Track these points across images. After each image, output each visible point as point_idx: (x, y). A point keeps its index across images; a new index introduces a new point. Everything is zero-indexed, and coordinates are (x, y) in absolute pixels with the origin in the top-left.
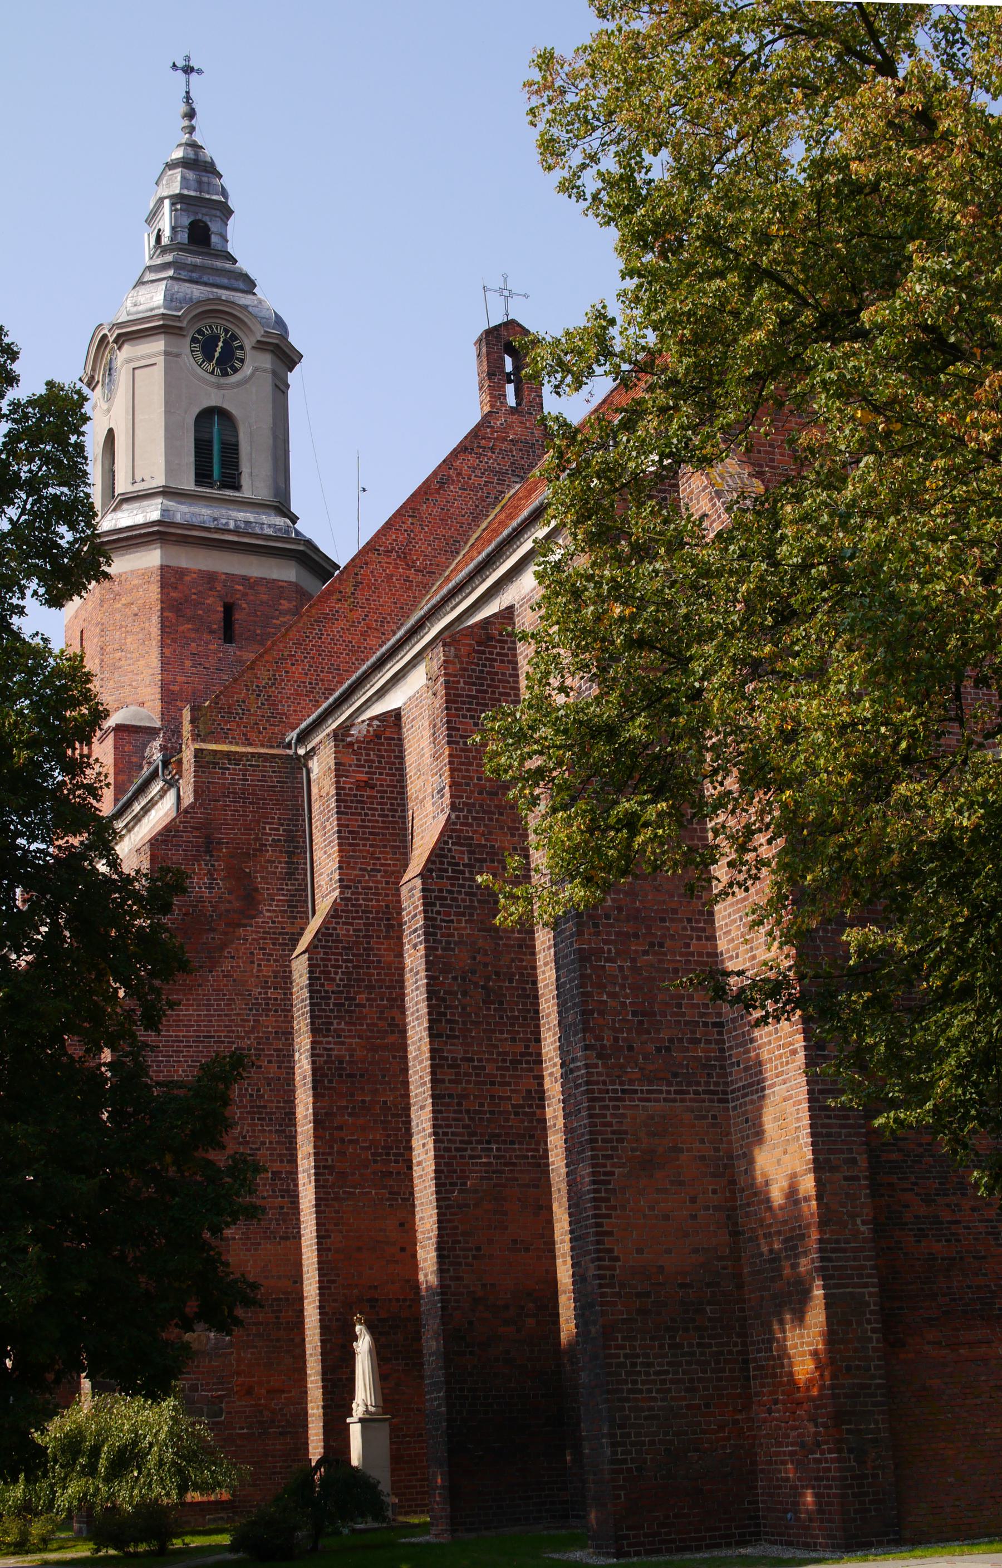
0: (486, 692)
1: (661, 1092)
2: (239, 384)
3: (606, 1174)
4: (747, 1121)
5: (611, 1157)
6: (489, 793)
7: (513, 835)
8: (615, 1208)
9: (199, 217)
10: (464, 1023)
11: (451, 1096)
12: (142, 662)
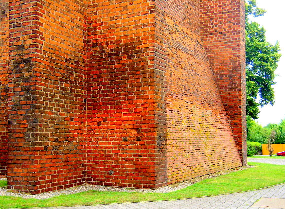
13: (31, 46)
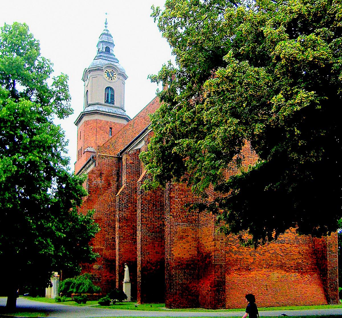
1: (185, 225)
2: (115, 82)
5: (174, 236)
8: (174, 246)
9: (108, 46)
10: (148, 210)
11: (145, 224)
12: (92, 138)
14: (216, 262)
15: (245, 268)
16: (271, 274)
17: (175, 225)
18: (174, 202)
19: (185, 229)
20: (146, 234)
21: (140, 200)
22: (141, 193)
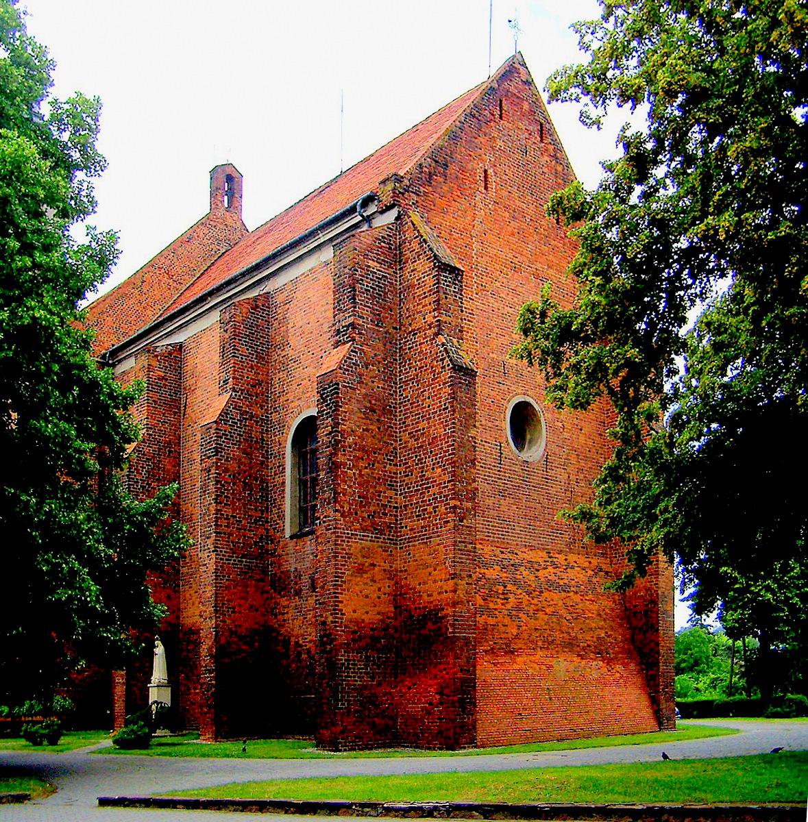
0: (253, 334)
1: (368, 536)
3: (341, 573)
4: (409, 554)
5: (344, 565)
6: (251, 386)
7: (262, 409)
8: (344, 590)
10: (233, 499)
11: (225, 534)
13: (332, 622)
14: (456, 633)
15: (503, 649)
16: (554, 663)
17: (346, 537)
18: (344, 476)
19: (369, 549)
20: (227, 560)
21: (213, 471)
22: (217, 452)
